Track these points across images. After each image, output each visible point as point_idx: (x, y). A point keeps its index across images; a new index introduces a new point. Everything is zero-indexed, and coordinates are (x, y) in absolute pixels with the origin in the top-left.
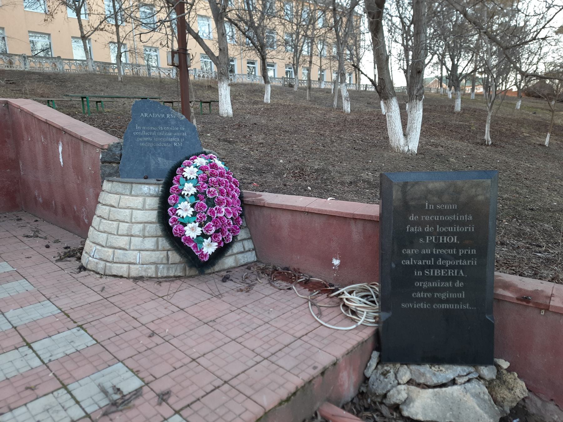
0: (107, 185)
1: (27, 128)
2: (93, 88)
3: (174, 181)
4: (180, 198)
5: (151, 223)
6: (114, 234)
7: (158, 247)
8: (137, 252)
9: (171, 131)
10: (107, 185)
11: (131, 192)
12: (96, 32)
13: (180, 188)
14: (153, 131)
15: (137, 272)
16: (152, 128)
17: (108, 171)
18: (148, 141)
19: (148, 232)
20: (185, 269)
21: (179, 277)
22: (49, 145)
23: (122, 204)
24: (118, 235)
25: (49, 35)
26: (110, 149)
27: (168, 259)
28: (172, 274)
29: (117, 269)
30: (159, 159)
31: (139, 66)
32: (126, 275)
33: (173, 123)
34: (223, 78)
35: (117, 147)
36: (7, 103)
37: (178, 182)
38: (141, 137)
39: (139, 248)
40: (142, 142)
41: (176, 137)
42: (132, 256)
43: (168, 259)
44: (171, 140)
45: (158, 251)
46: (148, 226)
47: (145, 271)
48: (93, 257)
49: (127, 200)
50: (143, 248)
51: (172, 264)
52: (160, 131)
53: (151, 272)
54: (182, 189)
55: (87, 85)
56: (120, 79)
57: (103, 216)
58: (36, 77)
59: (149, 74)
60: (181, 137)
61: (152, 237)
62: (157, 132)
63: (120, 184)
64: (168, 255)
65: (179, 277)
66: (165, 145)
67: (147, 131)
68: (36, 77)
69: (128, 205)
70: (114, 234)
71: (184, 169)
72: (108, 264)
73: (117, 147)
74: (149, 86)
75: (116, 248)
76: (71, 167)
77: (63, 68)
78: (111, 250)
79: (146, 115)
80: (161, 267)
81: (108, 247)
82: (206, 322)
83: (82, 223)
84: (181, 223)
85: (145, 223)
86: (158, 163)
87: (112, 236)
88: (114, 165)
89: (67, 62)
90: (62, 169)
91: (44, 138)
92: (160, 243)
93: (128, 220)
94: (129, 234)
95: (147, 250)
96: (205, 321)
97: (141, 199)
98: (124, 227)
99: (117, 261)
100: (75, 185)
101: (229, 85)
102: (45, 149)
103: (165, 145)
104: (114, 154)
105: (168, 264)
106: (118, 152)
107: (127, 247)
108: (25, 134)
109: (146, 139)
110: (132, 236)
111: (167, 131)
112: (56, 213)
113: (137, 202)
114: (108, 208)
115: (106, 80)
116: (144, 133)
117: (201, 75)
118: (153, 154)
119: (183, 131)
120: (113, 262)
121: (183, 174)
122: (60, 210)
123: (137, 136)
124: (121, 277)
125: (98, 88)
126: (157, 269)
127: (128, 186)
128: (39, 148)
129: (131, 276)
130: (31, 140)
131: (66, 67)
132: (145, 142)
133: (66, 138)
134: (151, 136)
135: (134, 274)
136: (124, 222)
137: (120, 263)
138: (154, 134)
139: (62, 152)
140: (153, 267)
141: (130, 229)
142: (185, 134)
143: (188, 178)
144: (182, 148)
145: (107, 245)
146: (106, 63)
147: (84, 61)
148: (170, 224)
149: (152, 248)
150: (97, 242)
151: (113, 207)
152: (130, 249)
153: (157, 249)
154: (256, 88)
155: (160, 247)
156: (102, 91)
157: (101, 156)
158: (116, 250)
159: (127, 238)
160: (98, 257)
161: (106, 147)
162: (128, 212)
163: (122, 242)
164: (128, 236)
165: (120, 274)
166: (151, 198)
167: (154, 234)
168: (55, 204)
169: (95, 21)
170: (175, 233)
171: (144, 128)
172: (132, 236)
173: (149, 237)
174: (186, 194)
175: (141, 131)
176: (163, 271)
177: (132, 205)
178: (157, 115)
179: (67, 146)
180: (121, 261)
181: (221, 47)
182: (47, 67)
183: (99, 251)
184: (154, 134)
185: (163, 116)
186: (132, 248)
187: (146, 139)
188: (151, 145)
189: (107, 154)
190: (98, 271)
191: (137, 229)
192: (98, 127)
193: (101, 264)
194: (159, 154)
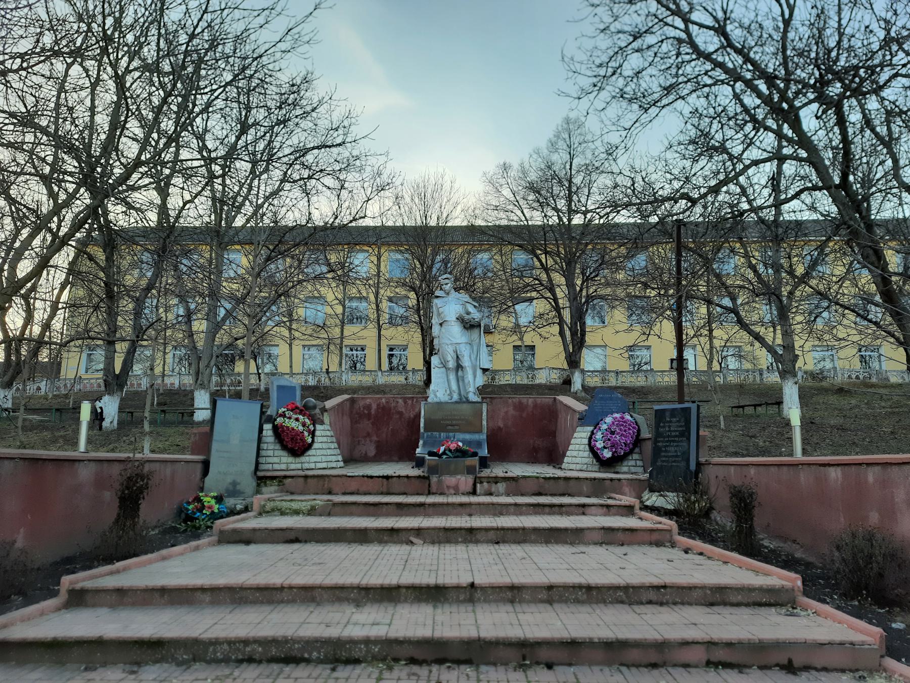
0: (579, 429)
34: (788, 376)
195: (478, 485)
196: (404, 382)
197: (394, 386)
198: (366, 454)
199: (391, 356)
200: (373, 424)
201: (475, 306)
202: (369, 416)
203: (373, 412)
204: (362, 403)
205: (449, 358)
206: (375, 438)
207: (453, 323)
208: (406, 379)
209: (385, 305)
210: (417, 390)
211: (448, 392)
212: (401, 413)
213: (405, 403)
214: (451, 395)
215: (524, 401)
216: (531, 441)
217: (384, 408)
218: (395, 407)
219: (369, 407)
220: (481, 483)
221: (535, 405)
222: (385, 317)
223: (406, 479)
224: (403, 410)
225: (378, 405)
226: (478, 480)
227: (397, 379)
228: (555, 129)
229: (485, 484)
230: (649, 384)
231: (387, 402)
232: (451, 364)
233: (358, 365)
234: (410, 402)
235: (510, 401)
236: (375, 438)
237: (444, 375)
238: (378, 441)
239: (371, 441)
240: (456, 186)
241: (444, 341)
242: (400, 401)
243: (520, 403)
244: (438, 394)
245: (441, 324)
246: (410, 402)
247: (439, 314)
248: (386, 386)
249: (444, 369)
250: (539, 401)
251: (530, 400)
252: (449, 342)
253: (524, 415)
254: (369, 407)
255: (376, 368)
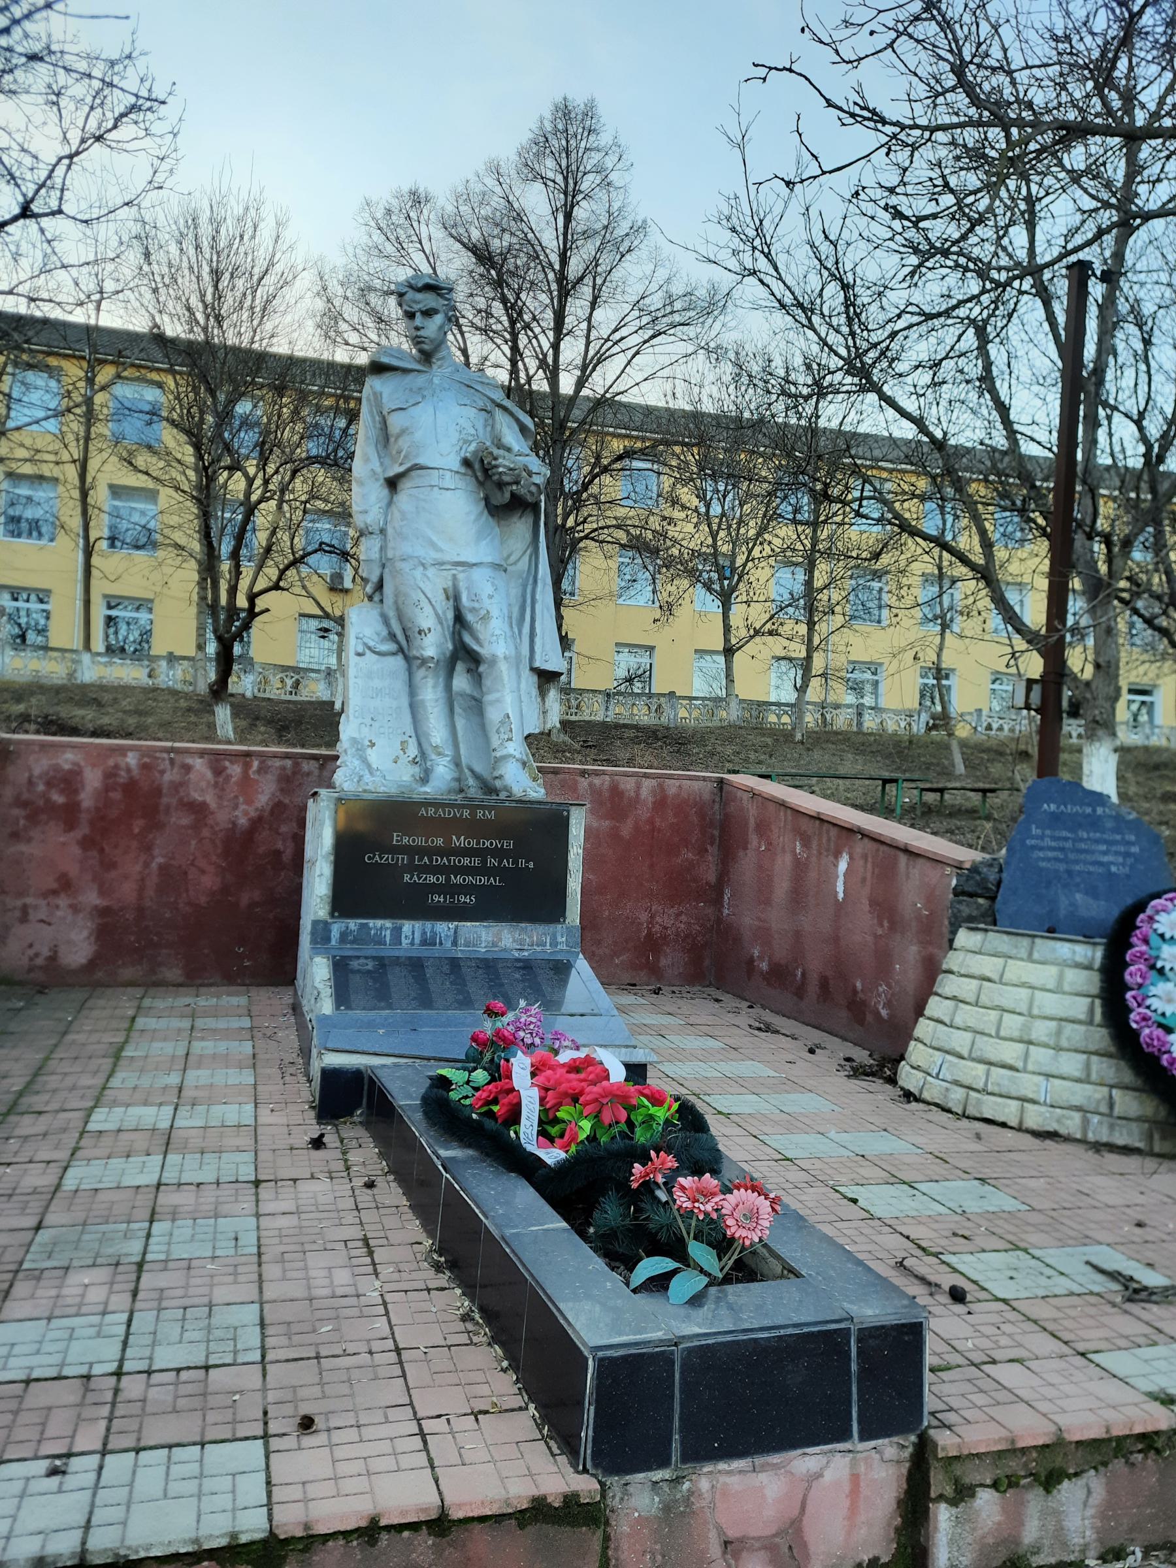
0: (964, 937)
1: (762, 828)
2: (742, 756)
3: (1134, 940)
4: (1154, 973)
5: (1073, 1022)
6: (990, 1035)
7: (1089, 1075)
8: (1041, 1078)
9: (1106, 842)
10: (964, 937)
11: (1030, 954)
12: (757, 639)
13: (1153, 953)
14: (1066, 839)
15: (1040, 1120)
16: (1065, 834)
17: (966, 910)
18: (1056, 859)
19: (1069, 1039)
20: (1150, 1138)
21: (1126, 1150)
22: (814, 859)
23: (1008, 976)
24: (998, 1037)
25: (651, 649)
26: (975, 869)
27: (1111, 1105)
28: (1120, 1141)
29: (991, 1107)
30: (1078, 896)
31: (837, 706)
32: (1013, 1122)
33: (1109, 824)
34: (1100, 733)
35: (991, 865)
36: (721, 782)
37: (1146, 941)
38: (1041, 849)
39: (1044, 1069)
40: (1043, 859)
41: (1117, 853)
42: (1029, 1085)
43: (1111, 1105)
44: (1105, 859)
45: (1089, 1083)
46: (1069, 1028)
47: (1058, 1121)
48: (937, 1077)
49: (1018, 970)
50: (1055, 1072)
51: (1120, 1118)
52: (1082, 840)
53: (1071, 1124)
54: (1157, 958)
55: (729, 750)
56: (798, 737)
57: (962, 996)
58: (631, 733)
59: (860, 724)
60: (1127, 855)
61: (1076, 1051)
62: (1074, 840)
63: (1005, 937)
64: (1111, 1097)
65: (1126, 1150)
66: (1091, 869)
67: (1053, 838)
68: (631, 733)
69: (1024, 980)
70: (990, 1035)
71: (1157, 918)
72: (972, 1094)
73: (991, 865)
74: (863, 753)
75: (991, 1064)
76: (866, 902)
77: (676, 715)
78: (981, 1068)
79: (1053, 807)
80: (1095, 1119)
81: (973, 1060)
82: (1081, 1350)
83: (869, 1018)
84: (1160, 1025)
85: (1061, 1020)
86: (1073, 904)
87: (986, 1038)
88: (981, 901)
89: (685, 702)
90: (839, 906)
91: (803, 846)
92: (1094, 1068)
93: (1024, 1010)
94: (1026, 1038)
95: (1064, 1078)
96: (1081, 1347)
97: (1053, 970)
98: (1012, 1023)
99: (996, 1090)
100: (869, 939)
101: (1116, 750)
102: (800, 866)
103: (1091, 869)
104: (985, 880)
105: (1110, 1115)
106: (993, 877)
107: (1020, 1065)
108: (754, 839)
109: (1050, 854)
110: (1030, 1043)
111: (1097, 841)
112: (800, 992)
113: (1046, 975)
114: (975, 983)
115: (769, 741)
116: (1048, 842)
117: (995, 726)
118: (1065, 886)
119: (1133, 844)
120: (984, 1091)
121: (1156, 926)
122: (813, 989)
123: (1034, 848)
124: (1004, 1125)
125: (752, 756)
126: (1085, 1123)
127: (1025, 942)
128: (783, 865)
129: (1025, 1126)
130: (767, 849)
131: (683, 713)
132: (1049, 860)
133: (861, 846)
134: (1062, 849)
135: (1031, 1122)
136: (1013, 1012)
137: (1001, 1096)
138: (1069, 845)
139: (845, 875)
140: (1077, 1116)
141: (1026, 1028)
142: (1135, 849)
143: (1168, 936)
144: (1128, 876)
145: (974, 1055)
146: (760, 704)
147: (720, 699)
148: (1134, 1026)
149: (1077, 1074)
150: (947, 1047)
151: (989, 980)
152: (1025, 1071)
153: (1085, 1080)
154: (1156, 759)
155: (1094, 1077)
156: (760, 762)
157: (954, 882)
158: (993, 1068)
159: (1021, 1046)
160: (949, 1078)
161: (968, 866)
162: (1024, 993)
163: (1010, 1052)
164: (1021, 1041)
165: (1001, 1119)
166: (1076, 971)
167: (1081, 1045)
168: (803, 974)
169: (758, 615)
170: (1148, 1045)
171: (1048, 832)
172: (1030, 1043)
173: (1068, 1050)
174: (1167, 968)
175: (1042, 837)
176: (1099, 1131)
177: (1032, 980)
178: (1077, 809)
179: (861, 863)
180: (1004, 1091)
181: (1101, 661)
182: (642, 715)
183: (951, 1064)
184: (1069, 845)
185: (1089, 810)
186: (1030, 1067)
187: (1050, 854)
188: (1062, 867)
189: (968, 878)
190: (950, 1105)
191: (1042, 1030)
192: (301, 875)
193: (958, 1094)
194: (1078, 885)
195: (943, 1516)
196: (146, 681)
197: (125, 690)
198: (53, 958)
199: (110, 620)
200: (87, 843)
201: (523, 429)
202: (69, 815)
203: (87, 799)
204: (40, 765)
205: (425, 619)
206: (91, 898)
207: (449, 481)
208: (150, 676)
209: (100, 496)
210: (183, 704)
211: (413, 751)
212: (199, 810)
213: (218, 771)
214: (422, 760)
215: (628, 785)
216: (644, 917)
217: (130, 788)
218: (176, 786)
219: (69, 781)
220: (962, 1494)
221: (661, 802)
222: (100, 529)
223: (426, 1540)
224: (210, 798)
225: (110, 775)
226: (939, 1483)
227: (129, 673)
228: (535, 126)
229: (986, 1499)
230: (664, 720)
231: (145, 767)
232: (433, 645)
233: (31, 636)
234: (235, 770)
235: (583, 783)
236: (91, 898)
237: (400, 685)
238: (104, 912)
239: (75, 909)
240: (288, 235)
241: (406, 548)
242: (198, 763)
243: (615, 791)
244: (373, 756)
245: (392, 484)
246: (235, 770)
247: (385, 437)
248: (103, 688)
249: (399, 661)
250: (672, 787)
251: (647, 784)
252: (430, 556)
253: (626, 830)
254: (69, 781)
255: (77, 643)
